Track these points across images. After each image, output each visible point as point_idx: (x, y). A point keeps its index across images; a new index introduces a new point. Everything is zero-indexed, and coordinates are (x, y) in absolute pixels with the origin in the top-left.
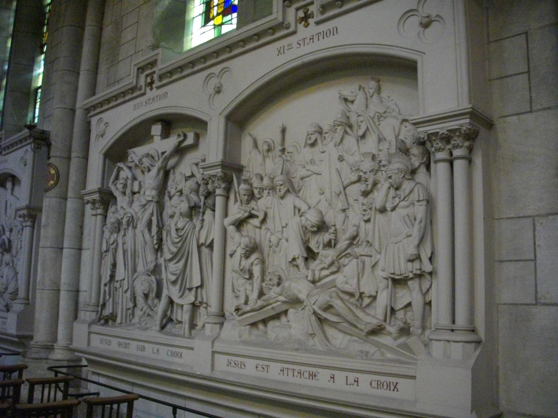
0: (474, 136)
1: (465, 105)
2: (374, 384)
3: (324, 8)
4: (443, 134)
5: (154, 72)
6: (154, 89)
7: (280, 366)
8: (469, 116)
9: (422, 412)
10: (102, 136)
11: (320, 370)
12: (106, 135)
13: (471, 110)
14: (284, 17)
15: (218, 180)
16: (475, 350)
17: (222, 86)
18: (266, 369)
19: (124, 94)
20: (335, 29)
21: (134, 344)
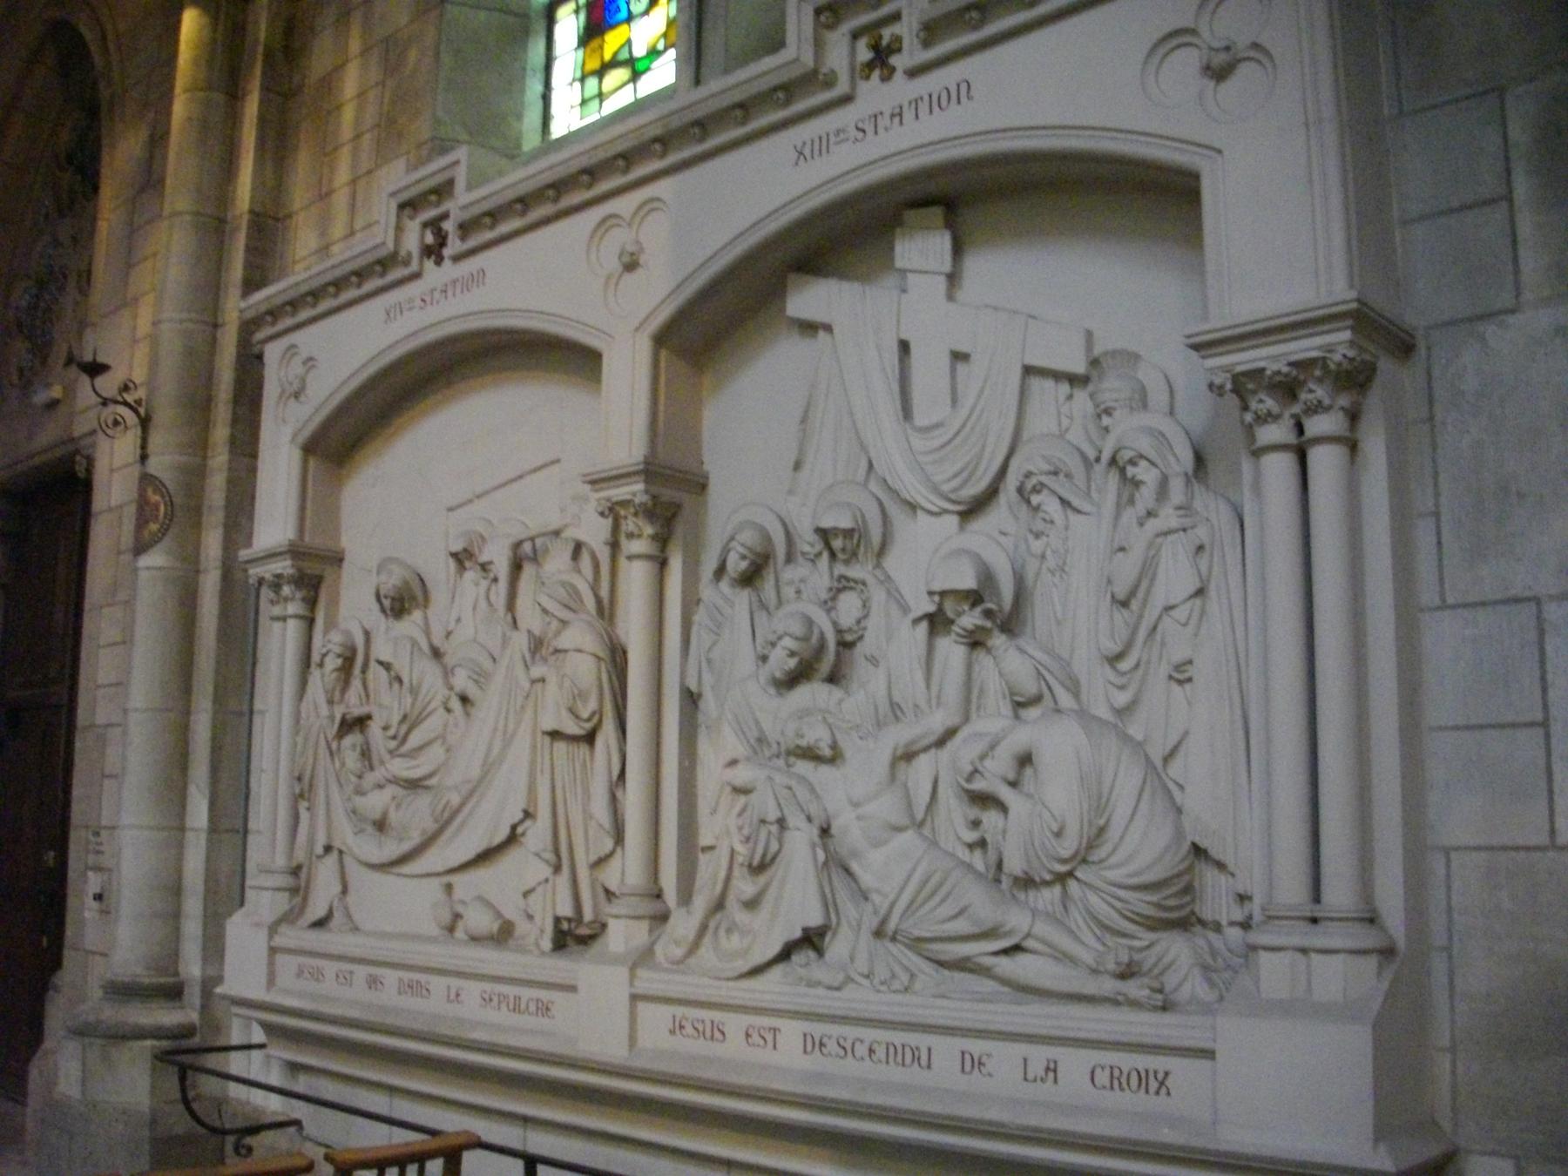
0: (1361, 378)
1: (1338, 290)
2: (1103, 1078)
3: (931, 31)
4: (1279, 373)
5: (445, 216)
6: (447, 263)
7: (666, 1011)
10: (297, 395)
12: (309, 391)
13: (1354, 305)
14: (397, 240)
15: (636, 514)
16: (1379, 974)
17: (641, 250)
18: (769, 1037)
20: (964, 88)
21: (438, 984)
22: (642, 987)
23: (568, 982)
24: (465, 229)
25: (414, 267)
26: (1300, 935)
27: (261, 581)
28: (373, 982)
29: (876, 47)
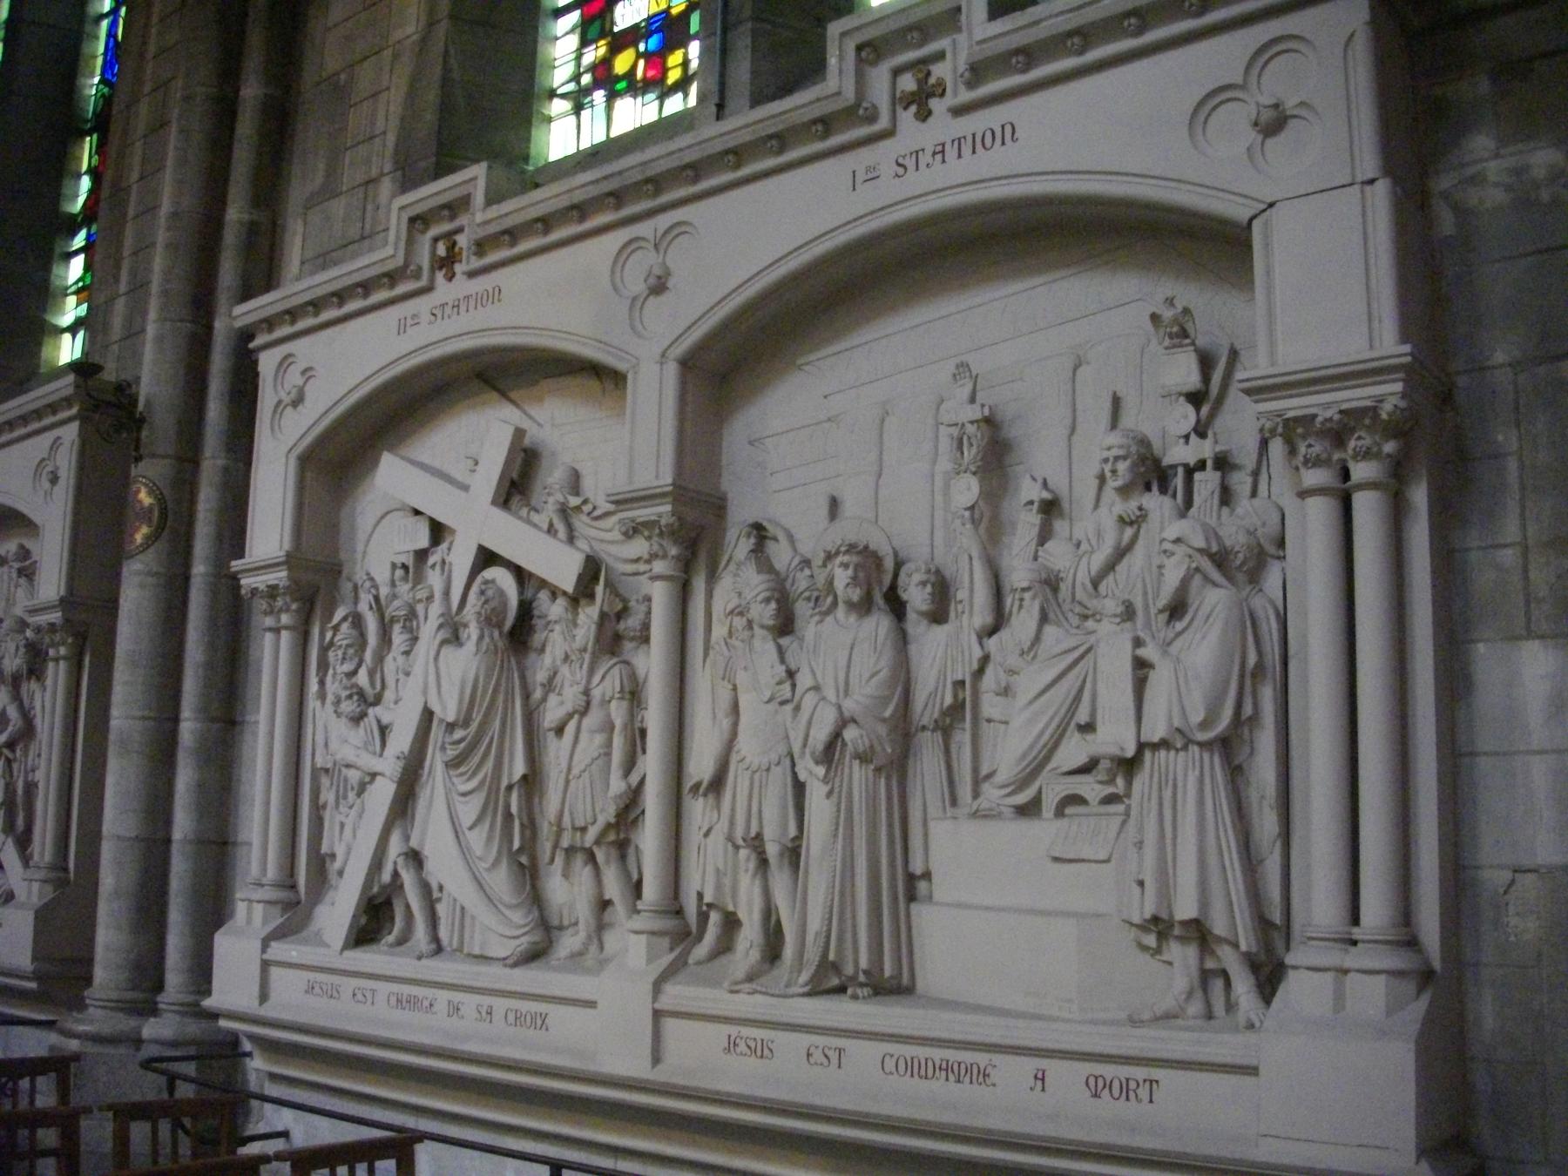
4: (1331, 419)
8: (1401, 375)
9: (1272, 1160)
11: (997, 1059)
13: (1409, 359)
15: (661, 534)
16: (1419, 992)
17: (668, 273)
18: (834, 1060)
19: (366, 287)
20: (1008, 129)
22: (665, 1003)
23: (1245, 1061)
24: (481, 247)
25: (883, 123)
26: (1334, 957)
27: (254, 591)
28: (455, 1009)
29: (922, 82)
